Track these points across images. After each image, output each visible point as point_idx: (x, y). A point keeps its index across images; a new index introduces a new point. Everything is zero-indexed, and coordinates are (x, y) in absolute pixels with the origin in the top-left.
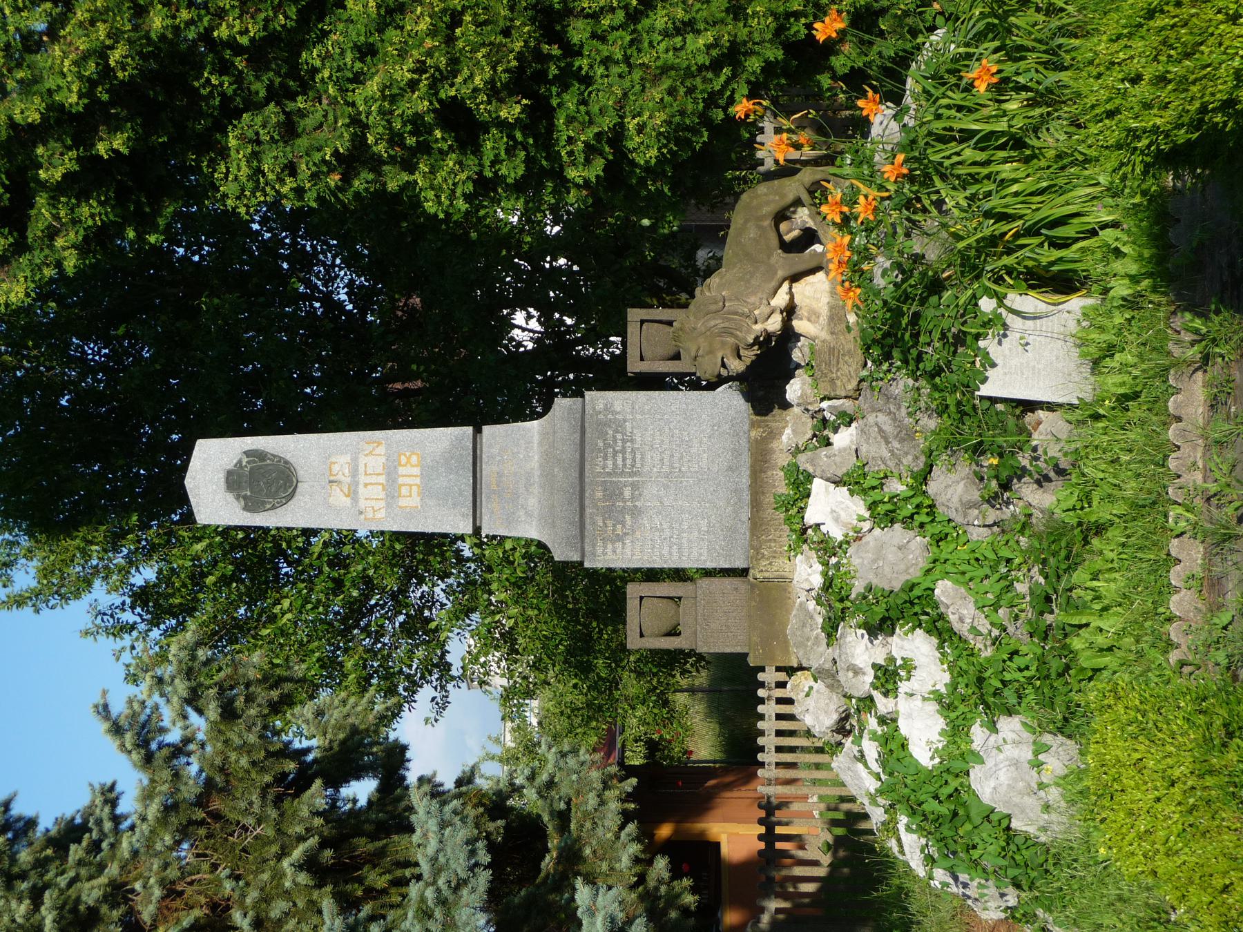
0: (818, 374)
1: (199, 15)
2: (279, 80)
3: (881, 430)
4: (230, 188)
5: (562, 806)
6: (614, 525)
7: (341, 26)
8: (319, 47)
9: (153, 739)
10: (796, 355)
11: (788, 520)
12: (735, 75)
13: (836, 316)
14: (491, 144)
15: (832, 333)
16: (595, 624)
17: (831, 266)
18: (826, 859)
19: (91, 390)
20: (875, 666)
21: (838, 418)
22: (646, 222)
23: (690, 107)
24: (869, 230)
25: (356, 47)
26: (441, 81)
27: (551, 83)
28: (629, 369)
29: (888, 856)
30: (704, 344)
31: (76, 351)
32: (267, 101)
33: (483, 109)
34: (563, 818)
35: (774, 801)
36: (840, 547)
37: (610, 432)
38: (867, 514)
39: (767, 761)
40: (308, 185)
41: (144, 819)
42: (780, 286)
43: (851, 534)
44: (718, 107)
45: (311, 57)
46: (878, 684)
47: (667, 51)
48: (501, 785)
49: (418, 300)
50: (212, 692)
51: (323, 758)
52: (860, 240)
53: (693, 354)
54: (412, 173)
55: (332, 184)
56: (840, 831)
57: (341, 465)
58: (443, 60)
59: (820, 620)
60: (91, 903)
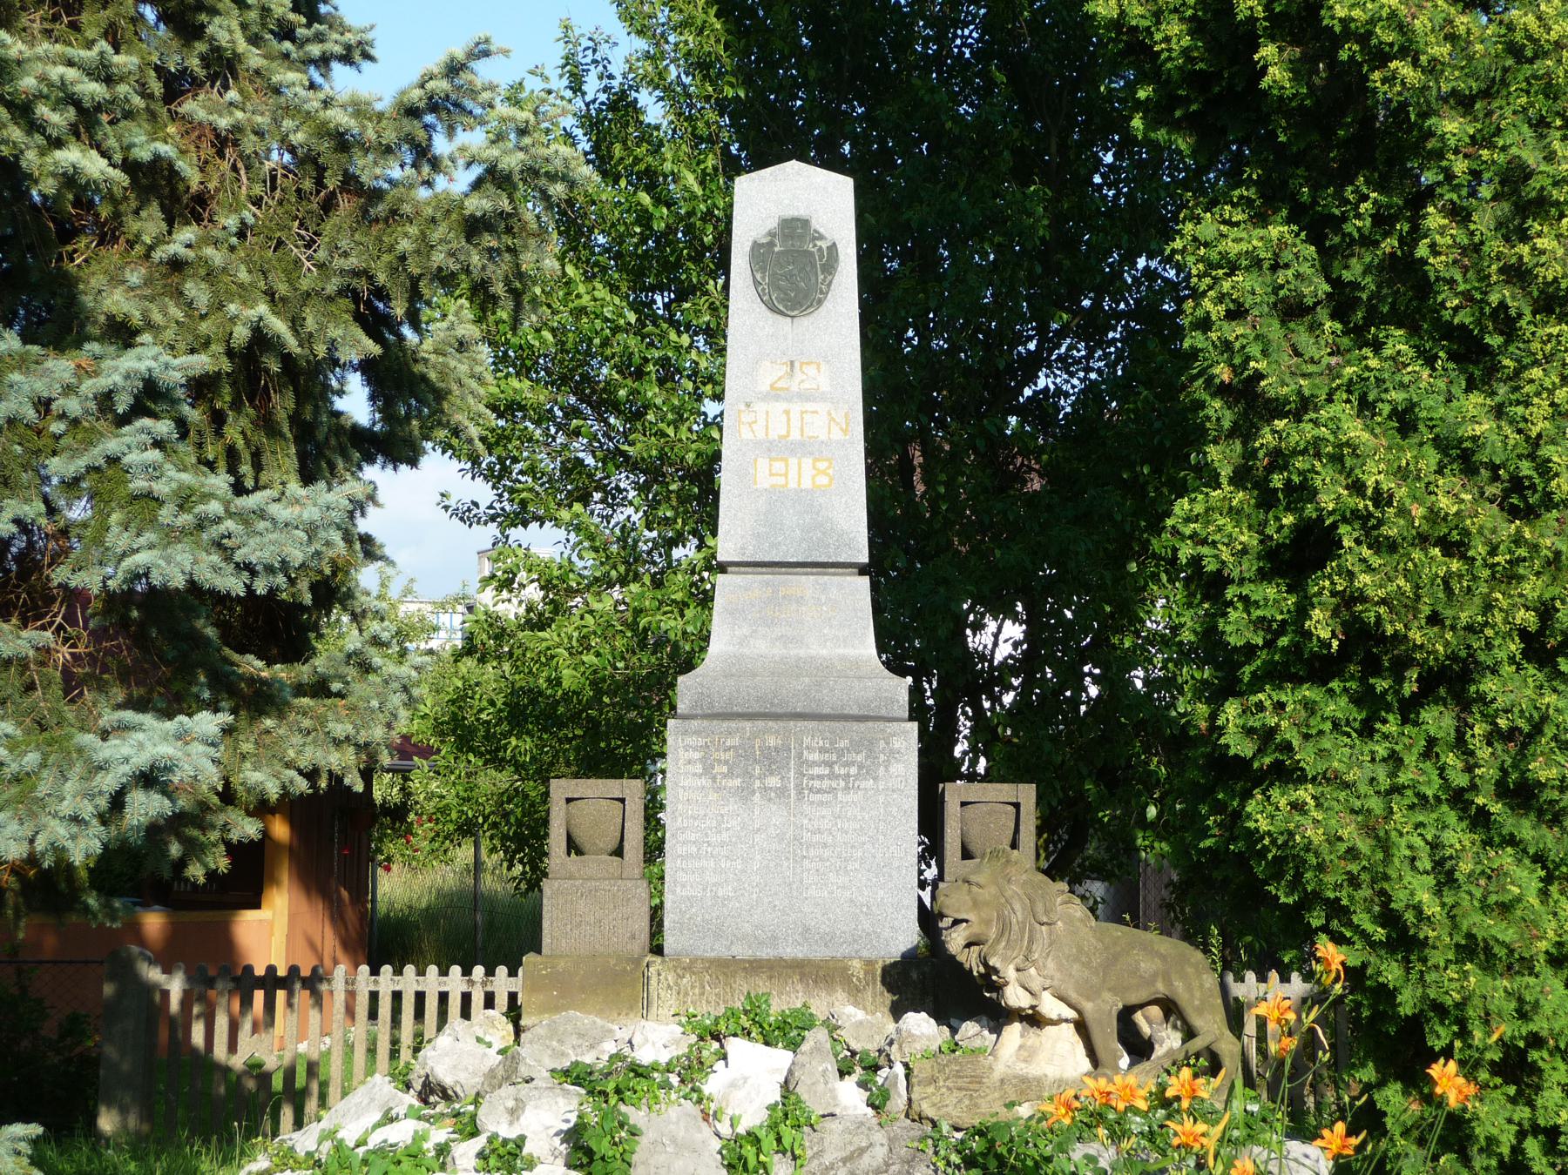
0: (943, 1059)
1: (1460, 186)
2: (1364, 297)
3: (862, 1151)
4: (1208, 227)
5: (336, 686)
6: (726, 762)
7: (1441, 384)
8: (1411, 353)
9: (440, 119)
10: (969, 1028)
11: (732, 1014)
12: (1373, 945)
13: (1027, 1087)
14: (1273, 597)
15: (1002, 1081)
16: (579, 732)
17: (1102, 1082)
18: (238, 1062)
19: (912, 38)
20: (520, 1142)
21: (879, 1088)
22: (1152, 812)
23: (1329, 879)
24: (1151, 1136)
25: (1411, 406)
26: (1364, 526)
27: (1363, 680)
28: (949, 785)
29: (242, 1153)
30: (985, 894)
31: (968, 13)
32: (1336, 283)
33: (1323, 585)
34: (320, 688)
35: (324, 987)
36: (693, 1090)
37: (860, 758)
38: (741, 1130)
39: (381, 978)
40: (1213, 336)
41: (327, 103)
42: (1070, 1006)
43: (713, 1106)
44: (1328, 919)
45: (1397, 342)
46: (496, 1144)
47: (1410, 847)
48: (363, 598)
49: (1037, 486)
50: (505, 204)
51: (403, 349)
52: (1136, 1124)
53: (973, 878)
54: (1231, 481)
55: (1216, 370)
56: (277, 1083)
57: (815, 378)
58: (1393, 532)
59: (588, 1059)
60: (210, 30)
